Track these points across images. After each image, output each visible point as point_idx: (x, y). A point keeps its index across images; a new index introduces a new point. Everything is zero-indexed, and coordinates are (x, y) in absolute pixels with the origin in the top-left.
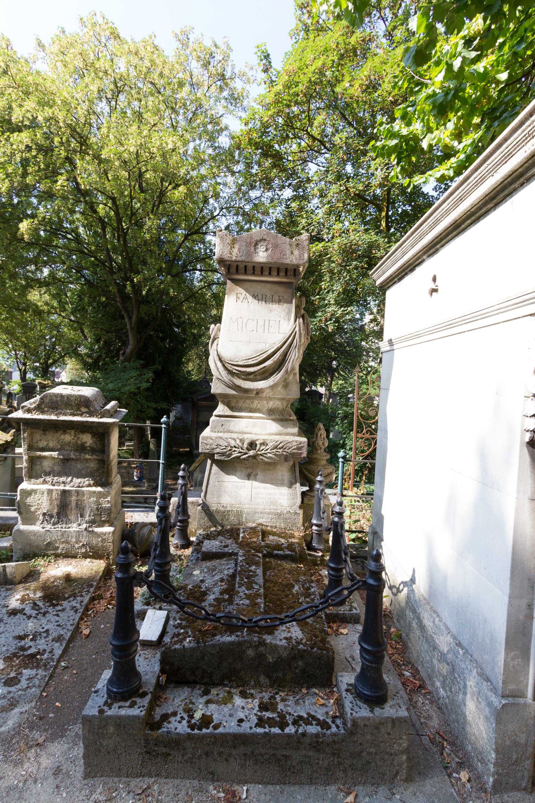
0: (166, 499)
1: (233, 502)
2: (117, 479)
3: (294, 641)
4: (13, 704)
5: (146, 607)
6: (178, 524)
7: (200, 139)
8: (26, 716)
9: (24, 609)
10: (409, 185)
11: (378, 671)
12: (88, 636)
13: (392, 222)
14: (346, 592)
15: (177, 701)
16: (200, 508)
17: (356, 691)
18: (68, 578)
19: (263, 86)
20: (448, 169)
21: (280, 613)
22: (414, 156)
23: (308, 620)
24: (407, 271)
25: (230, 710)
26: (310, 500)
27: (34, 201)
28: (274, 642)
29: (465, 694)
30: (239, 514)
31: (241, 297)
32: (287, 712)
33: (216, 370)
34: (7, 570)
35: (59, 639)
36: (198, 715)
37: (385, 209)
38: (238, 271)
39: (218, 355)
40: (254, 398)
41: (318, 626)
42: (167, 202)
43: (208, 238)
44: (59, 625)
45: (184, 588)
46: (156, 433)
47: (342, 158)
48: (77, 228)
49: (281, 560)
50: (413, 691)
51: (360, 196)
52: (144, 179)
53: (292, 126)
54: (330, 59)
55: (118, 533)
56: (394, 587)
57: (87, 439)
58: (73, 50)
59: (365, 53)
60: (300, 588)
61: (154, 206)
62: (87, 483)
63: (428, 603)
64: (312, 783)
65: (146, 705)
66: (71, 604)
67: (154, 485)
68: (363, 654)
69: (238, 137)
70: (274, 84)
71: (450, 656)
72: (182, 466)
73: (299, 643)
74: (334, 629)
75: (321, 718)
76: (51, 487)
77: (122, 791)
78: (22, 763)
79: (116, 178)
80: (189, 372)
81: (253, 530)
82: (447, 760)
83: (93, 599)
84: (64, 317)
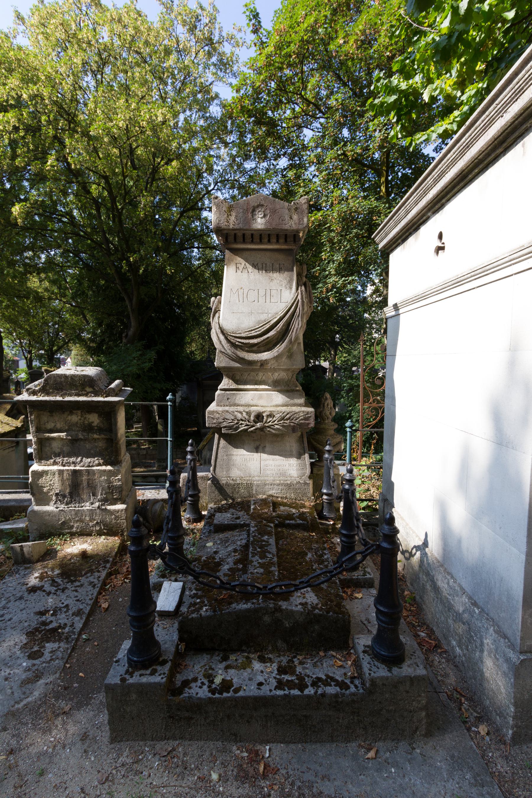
0: (176, 473)
1: (242, 475)
2: (126, 458)
3: (309, 607)
4: (38, 676)
5: (162, 580)
6: (189, 498)
7: (190, 110)
8: (51, 686)
9: (43, 586)
10: (411, 144)
11: (395, 632)
12: (107, 610)
13: (392, 187)
14: (359, 557)
15: (197, 668)
16: (209, 482)
17: (373, 652)
18: (84, 555)
19: (254, 48)
20: (452, 123)
21: (295, 580)
22: (415, 113)
23: (322, 586)
24: (411, 230)
25: (250, 674)
26: (319, 470)
27: (26, 184)
28: (290, 608)
29: (482, 651)
30: (249, 486)
32: (305, 675)
33: (218, 343)
34: (24, 549)
35: (79, 613)
36: (218, 680)
37: (385, 173)
38: (238, 241)
39: (220, 328)
40: (258, 370)
41: (332, 591)
42: (160, 179)
43: (205, 214)
44: (78, 600)
45: (198, 559)
46: (163, 411)
47: (339, 121)
48: (71, 211)
49: (293, 529)
50: (429, 651)
51: (357, 161)
52: (135, 156)
53: (285, 90)
54: (322, 14)
55: (131, 510)
56: (407, 551)
57: (94, 419)
58: (54, 20)
59: (359, 7)
60: (313, 556)
61: (147, 183)
62: (97, 462)
63: (442, 566)
64: (333, 741)
65: (167, 672)
66: (88, 579)
67: (164, 464)
68: (379, 616)
69: (230, 105)
70: (265, 45)
71: (466, 615)
72: (190, 442)
73: (314, 607)
74: (349, 593)
75: (340, 679)
76: (62, 468)
77: (148, 754)
78: (50, 730)
79: (108, 155)
80: (192, 352)
81: (264, 502)
82: (465, 715)
83: (109, 574)
84: (64, 303)
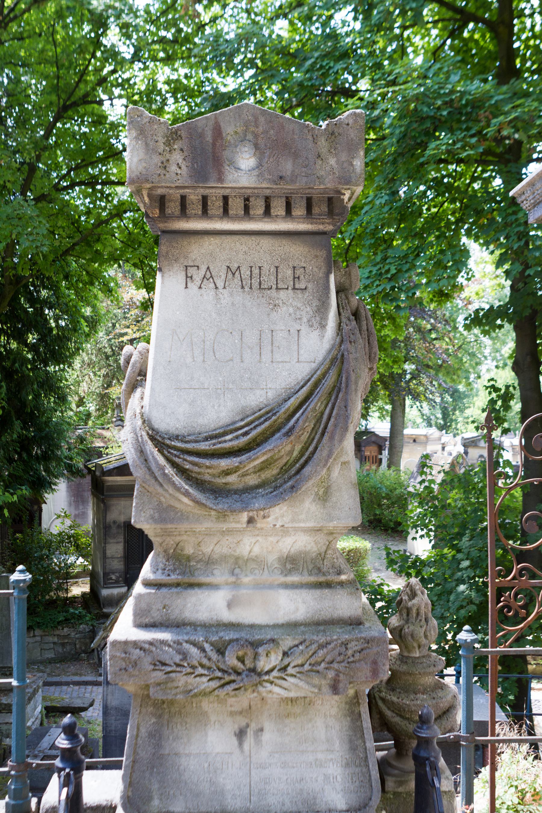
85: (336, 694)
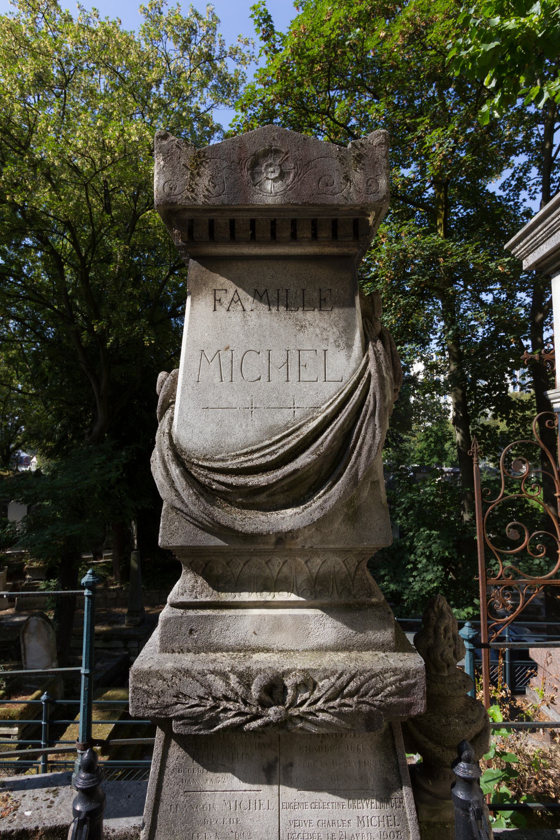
31: (226, 299)
33: (167, 487)
85: (371, 731)
